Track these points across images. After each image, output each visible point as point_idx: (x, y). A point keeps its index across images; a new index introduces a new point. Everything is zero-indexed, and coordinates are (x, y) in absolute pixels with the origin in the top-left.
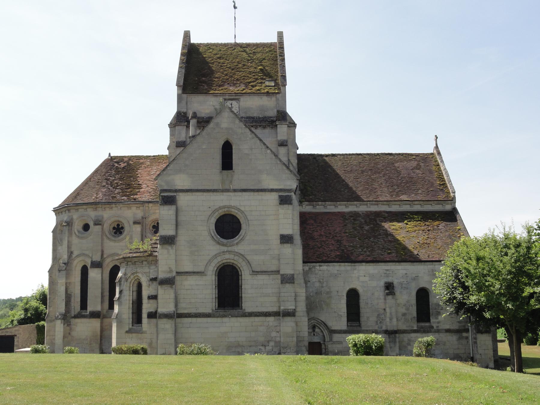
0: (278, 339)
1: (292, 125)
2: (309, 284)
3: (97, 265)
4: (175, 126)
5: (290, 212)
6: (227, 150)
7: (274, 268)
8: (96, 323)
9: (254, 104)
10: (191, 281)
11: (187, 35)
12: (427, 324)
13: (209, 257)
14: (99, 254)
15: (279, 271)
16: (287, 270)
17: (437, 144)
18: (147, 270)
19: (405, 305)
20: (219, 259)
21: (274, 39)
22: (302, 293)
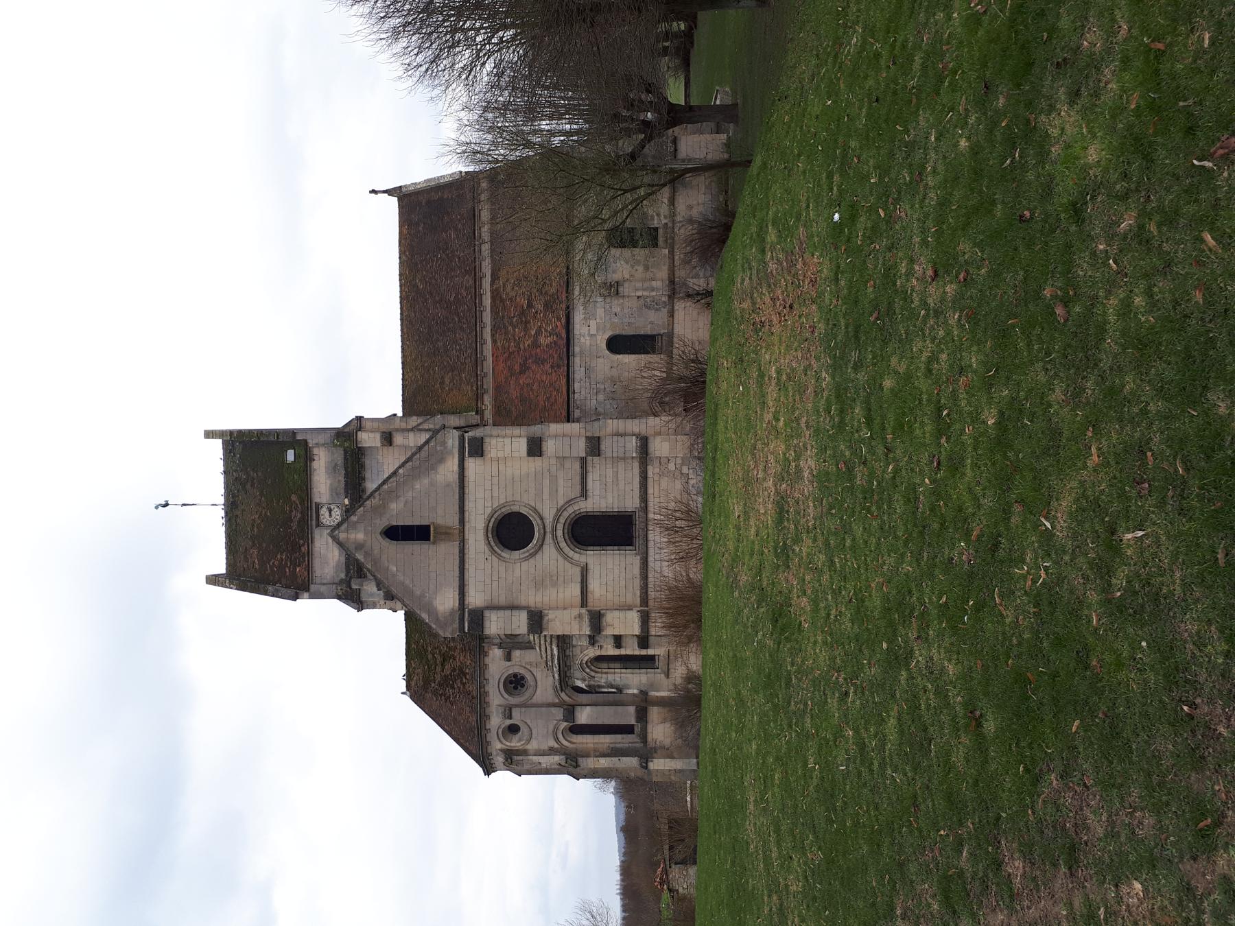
0: (679, 461)
1: (358, 422)
2: (600, 410)
3: (570, 712)
4: (361, 602)
5: (493, 441)
6: (397, 533)
7: (577, 465)
8: (654, 713)
9: (324, 481)
10: (596, 587)
11: (213, 580)
12: (661, 231)
13: (560, 559)
14: (554, 710)
15: (582, 458)
16: (580, 447)
17: (384, 192)
18: (578, 650)
19: (632, 267)
20: (563, 544)
21: (218, 443)
22: (612, 425)
